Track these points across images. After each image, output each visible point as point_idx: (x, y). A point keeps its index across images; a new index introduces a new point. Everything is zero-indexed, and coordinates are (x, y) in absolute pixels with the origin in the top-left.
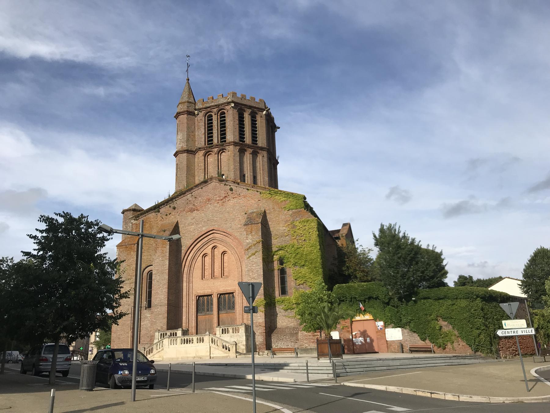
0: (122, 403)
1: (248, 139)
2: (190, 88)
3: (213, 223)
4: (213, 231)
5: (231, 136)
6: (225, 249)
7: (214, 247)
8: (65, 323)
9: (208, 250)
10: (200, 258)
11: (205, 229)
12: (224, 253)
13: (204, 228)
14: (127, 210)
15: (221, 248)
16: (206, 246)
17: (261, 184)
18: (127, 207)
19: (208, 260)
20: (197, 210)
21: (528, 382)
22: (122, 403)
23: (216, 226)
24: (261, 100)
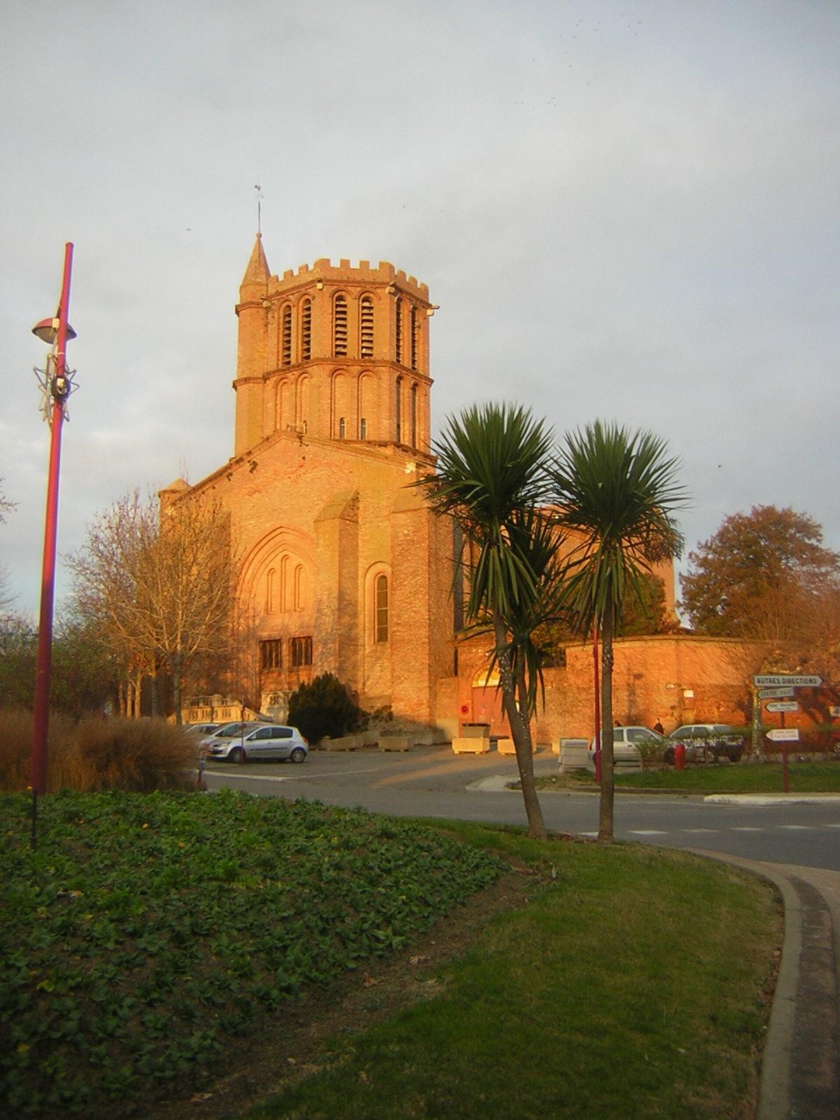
0: (70, 247)
1: (353, 350)
2: (259, 242)
3: (282, 515)
4: (282, 530)
5: (322, 344)
6: (300, 560)
7: (285, 557)
8: (103, 797)
9: (276, 564)
10: (264, 576)
11: (269, 526)
12: (299, 567)
13: (637, 645)
14: (165, 492)
15: (295, 560)
16: (272, 556)
17: (404, 441)
18: (164, 488)
19: (276, 578)
20: (259, 492)
21: (488, 685)
22: (70, 247)
23: (285, 521)
24: (381, 264)
